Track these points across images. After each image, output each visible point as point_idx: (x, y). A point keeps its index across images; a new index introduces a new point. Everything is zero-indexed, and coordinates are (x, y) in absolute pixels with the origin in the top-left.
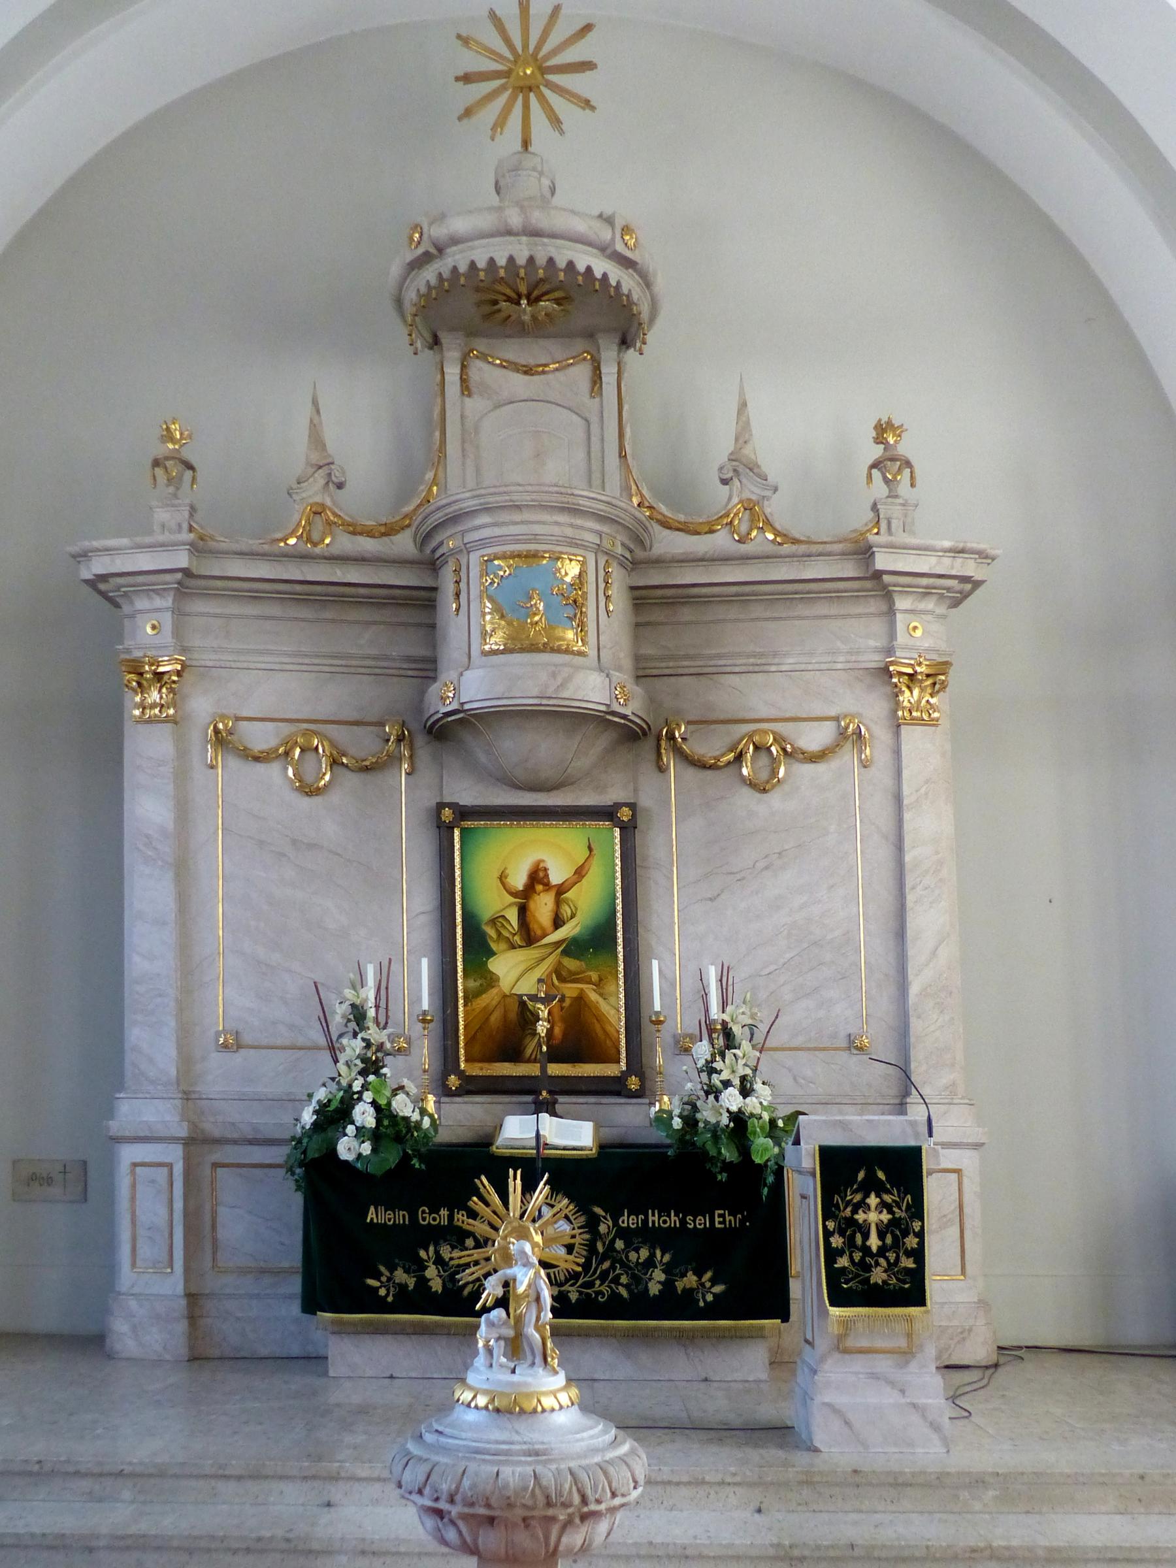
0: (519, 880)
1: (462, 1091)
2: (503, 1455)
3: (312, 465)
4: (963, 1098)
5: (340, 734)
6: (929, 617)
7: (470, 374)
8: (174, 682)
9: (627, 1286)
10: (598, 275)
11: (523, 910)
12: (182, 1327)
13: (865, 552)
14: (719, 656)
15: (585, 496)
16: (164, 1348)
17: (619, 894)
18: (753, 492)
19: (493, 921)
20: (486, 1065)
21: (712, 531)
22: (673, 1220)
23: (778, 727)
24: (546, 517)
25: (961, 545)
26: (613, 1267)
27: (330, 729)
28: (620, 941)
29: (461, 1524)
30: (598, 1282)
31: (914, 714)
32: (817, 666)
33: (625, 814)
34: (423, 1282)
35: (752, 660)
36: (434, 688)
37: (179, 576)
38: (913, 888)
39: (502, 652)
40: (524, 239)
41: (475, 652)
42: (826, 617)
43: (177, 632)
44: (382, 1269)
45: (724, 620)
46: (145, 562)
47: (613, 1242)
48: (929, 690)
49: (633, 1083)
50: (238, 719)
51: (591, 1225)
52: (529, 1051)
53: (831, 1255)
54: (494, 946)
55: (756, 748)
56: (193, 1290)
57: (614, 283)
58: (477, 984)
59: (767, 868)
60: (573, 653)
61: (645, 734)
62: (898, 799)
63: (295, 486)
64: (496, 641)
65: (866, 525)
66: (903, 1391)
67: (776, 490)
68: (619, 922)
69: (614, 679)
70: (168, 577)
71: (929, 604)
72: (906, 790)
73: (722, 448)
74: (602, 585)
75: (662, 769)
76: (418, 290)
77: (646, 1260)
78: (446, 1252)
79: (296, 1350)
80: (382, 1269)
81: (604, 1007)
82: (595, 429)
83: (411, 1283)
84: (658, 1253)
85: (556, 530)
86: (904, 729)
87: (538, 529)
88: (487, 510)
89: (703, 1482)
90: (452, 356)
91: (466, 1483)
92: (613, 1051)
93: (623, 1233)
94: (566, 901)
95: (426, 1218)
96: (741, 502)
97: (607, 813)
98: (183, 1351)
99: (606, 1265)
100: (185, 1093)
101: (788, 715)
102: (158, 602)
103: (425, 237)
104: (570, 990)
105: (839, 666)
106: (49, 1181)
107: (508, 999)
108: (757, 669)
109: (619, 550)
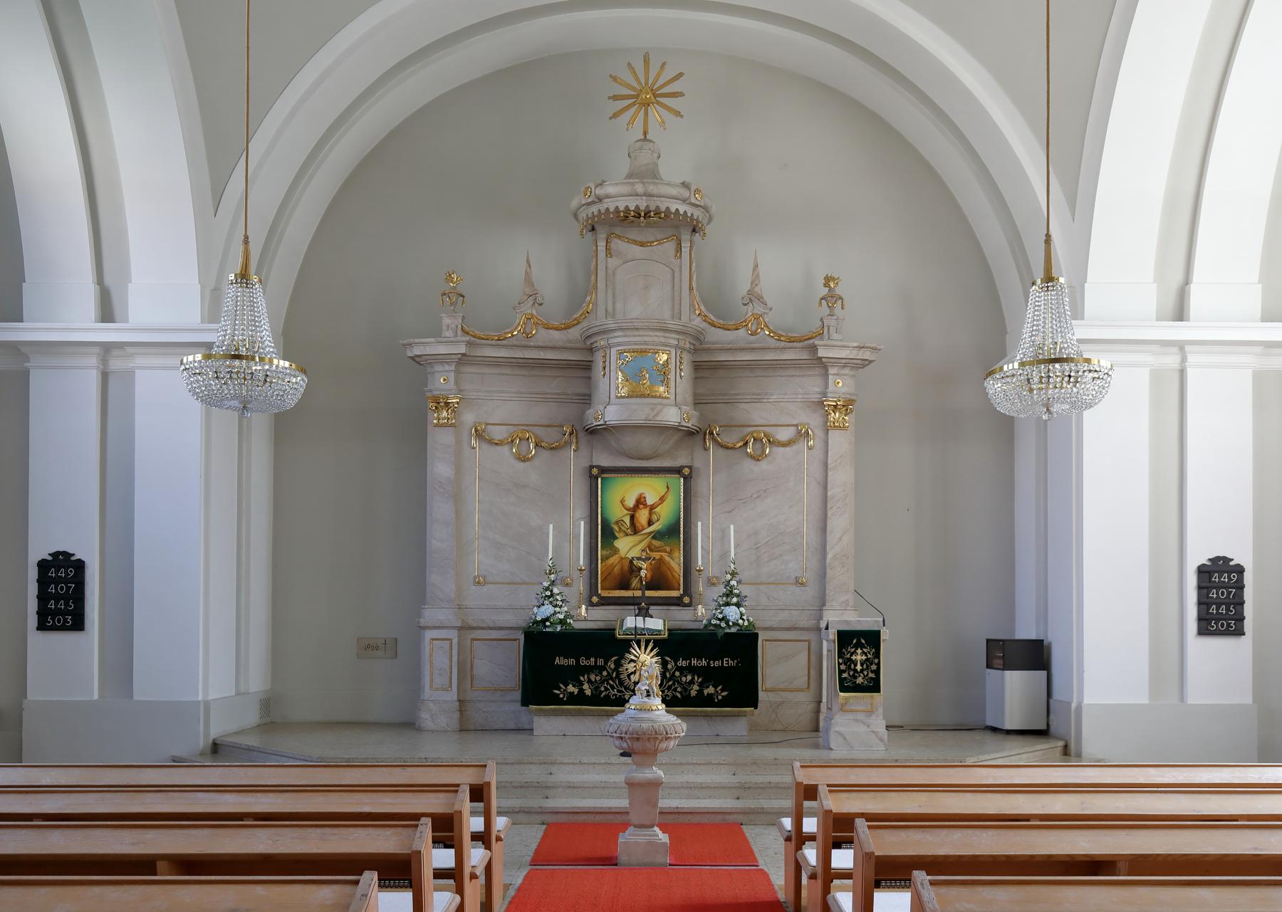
0: (631, 503)
1: (600, 604)
2: (642, 720)
3: (527, 295)
4: (852, 607)
5: (538, 430)
6: (846, 377)
7: (611, 246)
8: (456, 407)
9: (680, 693)
10: (682, 212)
11: (632, 517)
12: (457, 715)
13: (814, 349)
14: (738, 395)
15: (672, 324)
16: (447, 725)
17: (682, 510)
18: (759, 310)
19: (617, 523)
20: (612, 591)
21: (737, 329)
22: (704, 663)
23: (767, 429)
24: (652, 333)
25: (862, 345)
26: (674, 684)
27: (537, 430)
28: (682, 532)
29: (628, 741)
30: (666, 691)
31: (836, 424)
32: (788, 400)
33: (686, 471)
34: (581, 691)
35: (754, 397)
36: (590, 412)
37: (460, 356)
38: (831, 508)
39: (627, 397)
40: (644, 198)
41: (613, 396)
42: (793, 376)
43: (456, 382)
44: (561, 685)
45: (741, 377)
46: (442, 350)
47: (674, 672)
48: (844, 413)
49: (686, 600)
50: (487, 424)
51: (664, 664)
52: (633, 585)
53: (841, 672)
54: (617, 534)
55: (755, 439)
56: (461, 699)
57: (689, 215)
58: (608, 552)
59: (758, 497)
60: (663, 398)
61: (698, 432)
62: (826, 464)
63: (517, 305)
64: (624, 392)
65: (817, 329)
66: (868, 726)
67: (771, 309)
68: (682, 523)
69: (683, 410)
70: (453, 357)
71: (847, 371)
72: (829, 462)
73: (743, 288)
74: (678, 364)
75: (706, 449)
76: (587, 215)
77: (690, 681)
78: (593, 677)
79: (512, 726)
80: (561, 685)
81: (674, 564)
82: (677, 274)
83: (576, 691)
84: (696, 678)
85: (656, 339)
86: (830, 432)
87: (647, 339)
88: (621, 329)
89: (711, 764)
90: (602, 236)
91: (631, 728)
92: (676, 585)
93: (680, 669)
94: (655, 513)
95: (583, 662)
96: (753, 314)
97: (678, 471)
98: (457, 727)
99: (671, 683)
100: (458, 605)
101: (772, 423)
102: (447, 367)
103: (593, 193)
104: (657, 555)
105: (799, 400)
106: (377, 648)
107: (624, 560)
108: (757, 401)
109: (688, 346)
